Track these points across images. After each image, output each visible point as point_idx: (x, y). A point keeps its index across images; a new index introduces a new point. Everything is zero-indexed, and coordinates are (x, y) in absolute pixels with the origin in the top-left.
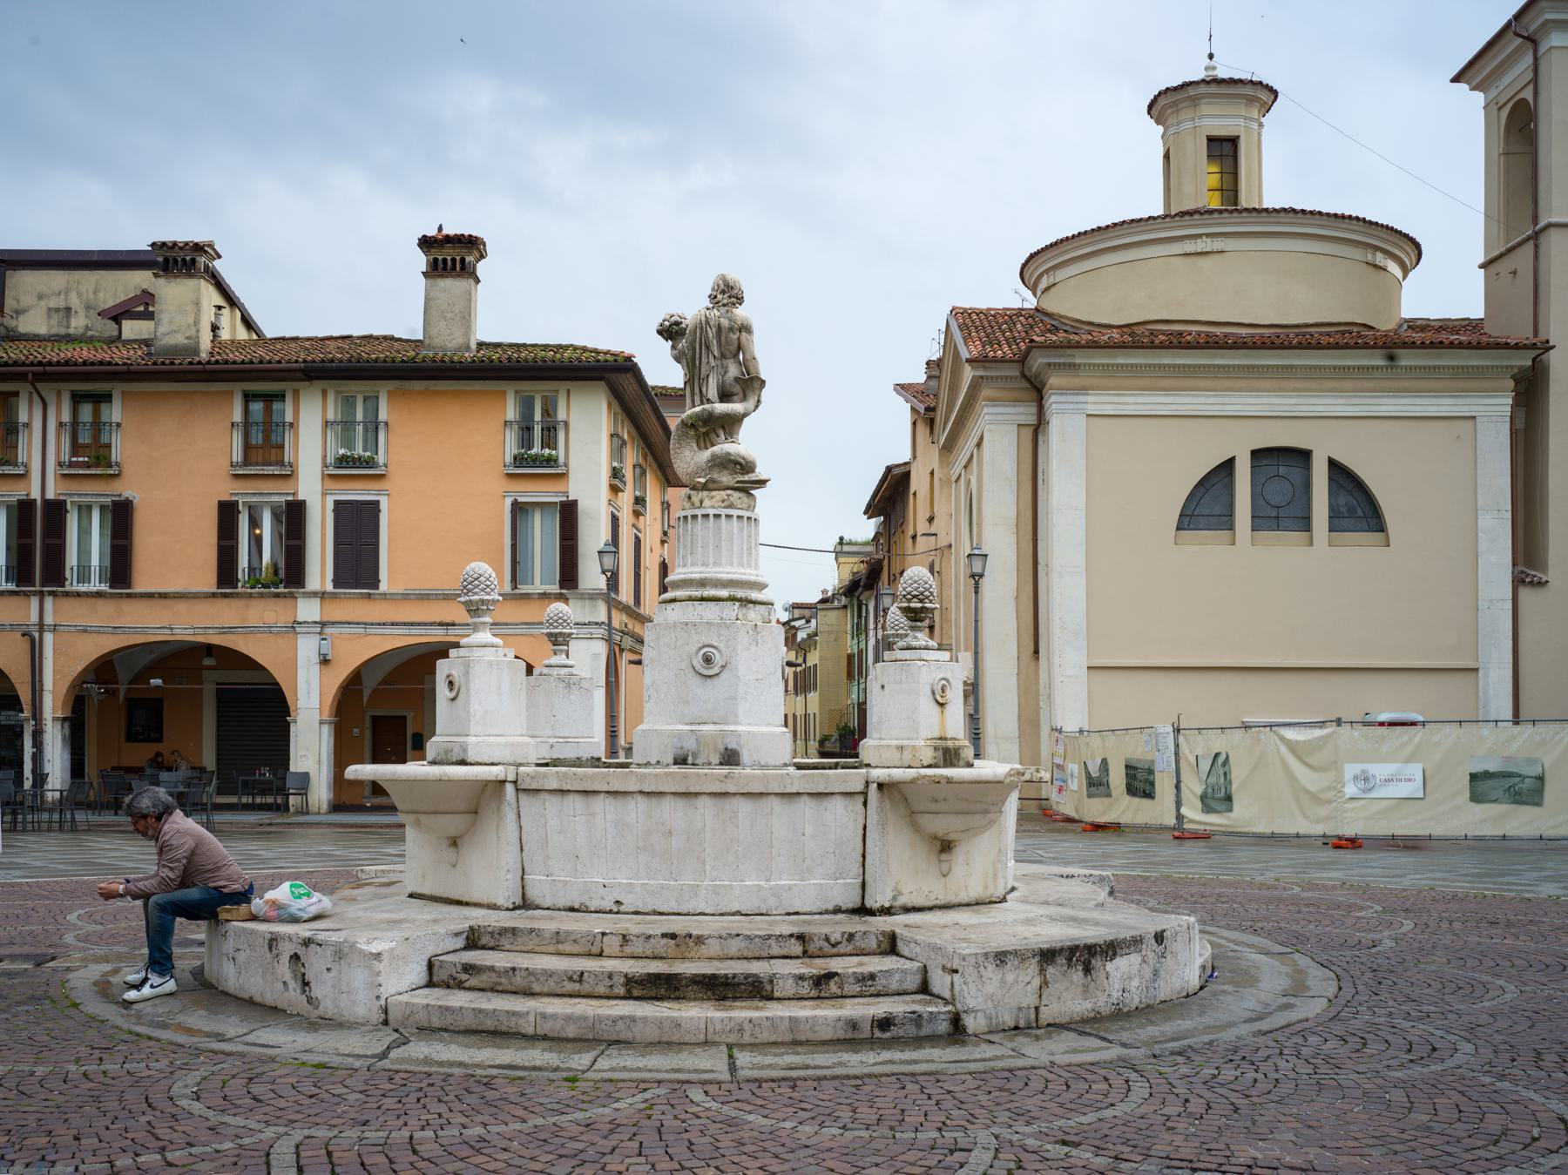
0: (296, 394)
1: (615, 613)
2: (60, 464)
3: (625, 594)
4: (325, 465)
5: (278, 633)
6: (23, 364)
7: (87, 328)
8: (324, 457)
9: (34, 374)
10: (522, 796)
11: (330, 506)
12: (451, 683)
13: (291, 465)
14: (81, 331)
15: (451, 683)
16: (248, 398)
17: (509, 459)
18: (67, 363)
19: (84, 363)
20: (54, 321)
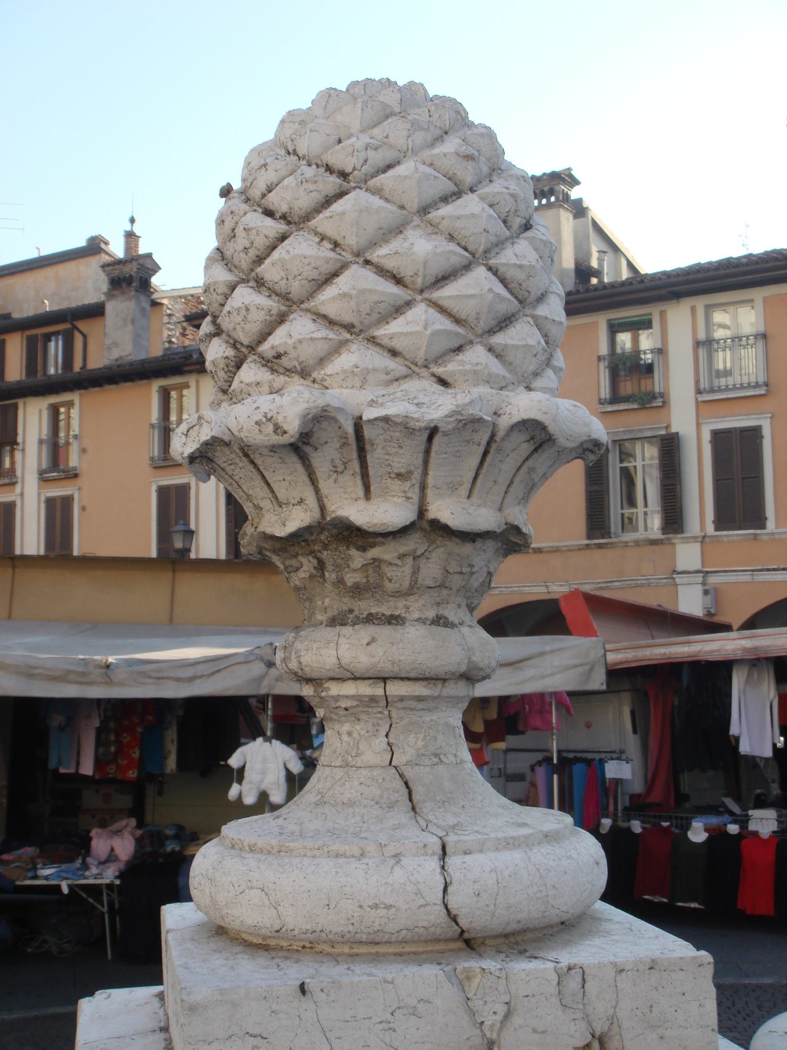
0: (663, 314)
8: (697, 382)
11: (706, 437)
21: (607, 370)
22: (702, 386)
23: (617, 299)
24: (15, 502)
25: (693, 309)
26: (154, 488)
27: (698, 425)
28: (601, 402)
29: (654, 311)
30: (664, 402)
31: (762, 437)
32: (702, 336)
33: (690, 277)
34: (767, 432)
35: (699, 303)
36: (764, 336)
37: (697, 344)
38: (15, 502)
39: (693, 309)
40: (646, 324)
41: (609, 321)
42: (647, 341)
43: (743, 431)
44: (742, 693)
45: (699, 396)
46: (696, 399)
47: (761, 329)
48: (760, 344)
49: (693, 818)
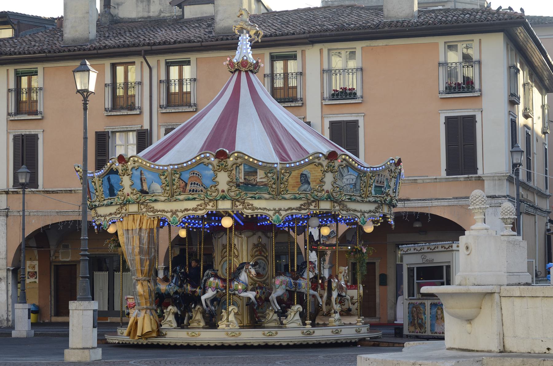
0: (303, 52)
1: (521, 190)
2: (161, 107)
3: (522, 176)
4: (323, 99)
5: (18, 91)
6: (139, 45)
7: (161, 12)
8: (322, 93)
9: (145, 51)
10: (503, 299)
11: (327, 125)
12: (467, 248)
13: (301, 99)
14: (156, 14)
15: (467, 248)
16: (274, 58)
17: (442, 88)
18: (164, 43)
19: (175, 42)
20: (140, 9)
21: (536, 65)
22: (325, 96)
23: (218, 47)
24: (37, 135)
25: (321, 51)
26: (443, 120)
27: (322, 117)
28: (106, 110)
29: (298, 50)
30: (302, 104)
31: (359, 127)
32: (326, 67)
33: (322, 33)
34: (361, 124)
35: (326, 47)
36: (362, 69)
37: (323, 71)
38: (37, 135)
39: (321, 51)
40: (294, 57)
41: (270, 53)
42: (293, 66)
43: (348, 122)
44: (157, 257)
45: (323, 101)
46: (322, 103)
47: (360, 65)
48: (359, 73)
49: (357, 354)
